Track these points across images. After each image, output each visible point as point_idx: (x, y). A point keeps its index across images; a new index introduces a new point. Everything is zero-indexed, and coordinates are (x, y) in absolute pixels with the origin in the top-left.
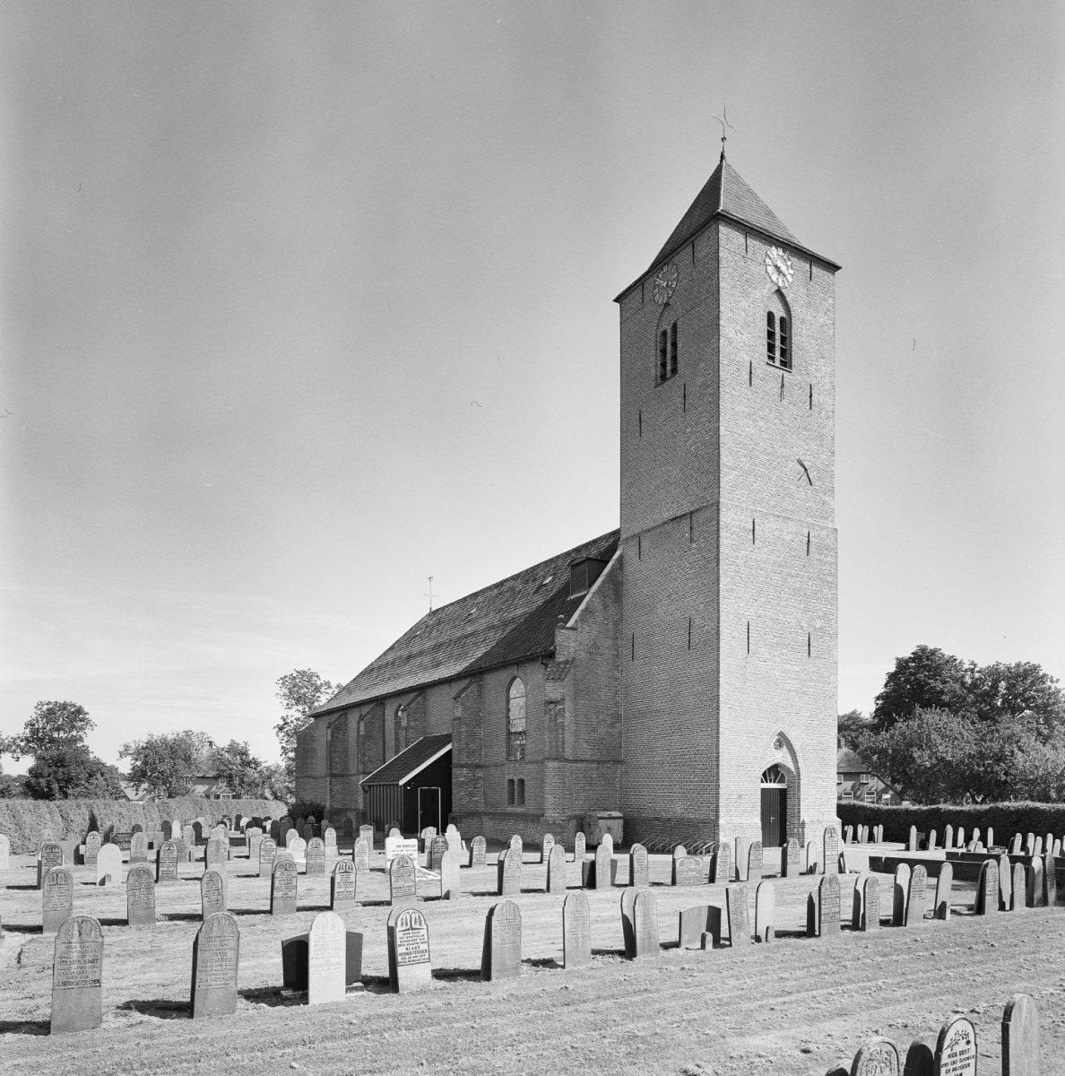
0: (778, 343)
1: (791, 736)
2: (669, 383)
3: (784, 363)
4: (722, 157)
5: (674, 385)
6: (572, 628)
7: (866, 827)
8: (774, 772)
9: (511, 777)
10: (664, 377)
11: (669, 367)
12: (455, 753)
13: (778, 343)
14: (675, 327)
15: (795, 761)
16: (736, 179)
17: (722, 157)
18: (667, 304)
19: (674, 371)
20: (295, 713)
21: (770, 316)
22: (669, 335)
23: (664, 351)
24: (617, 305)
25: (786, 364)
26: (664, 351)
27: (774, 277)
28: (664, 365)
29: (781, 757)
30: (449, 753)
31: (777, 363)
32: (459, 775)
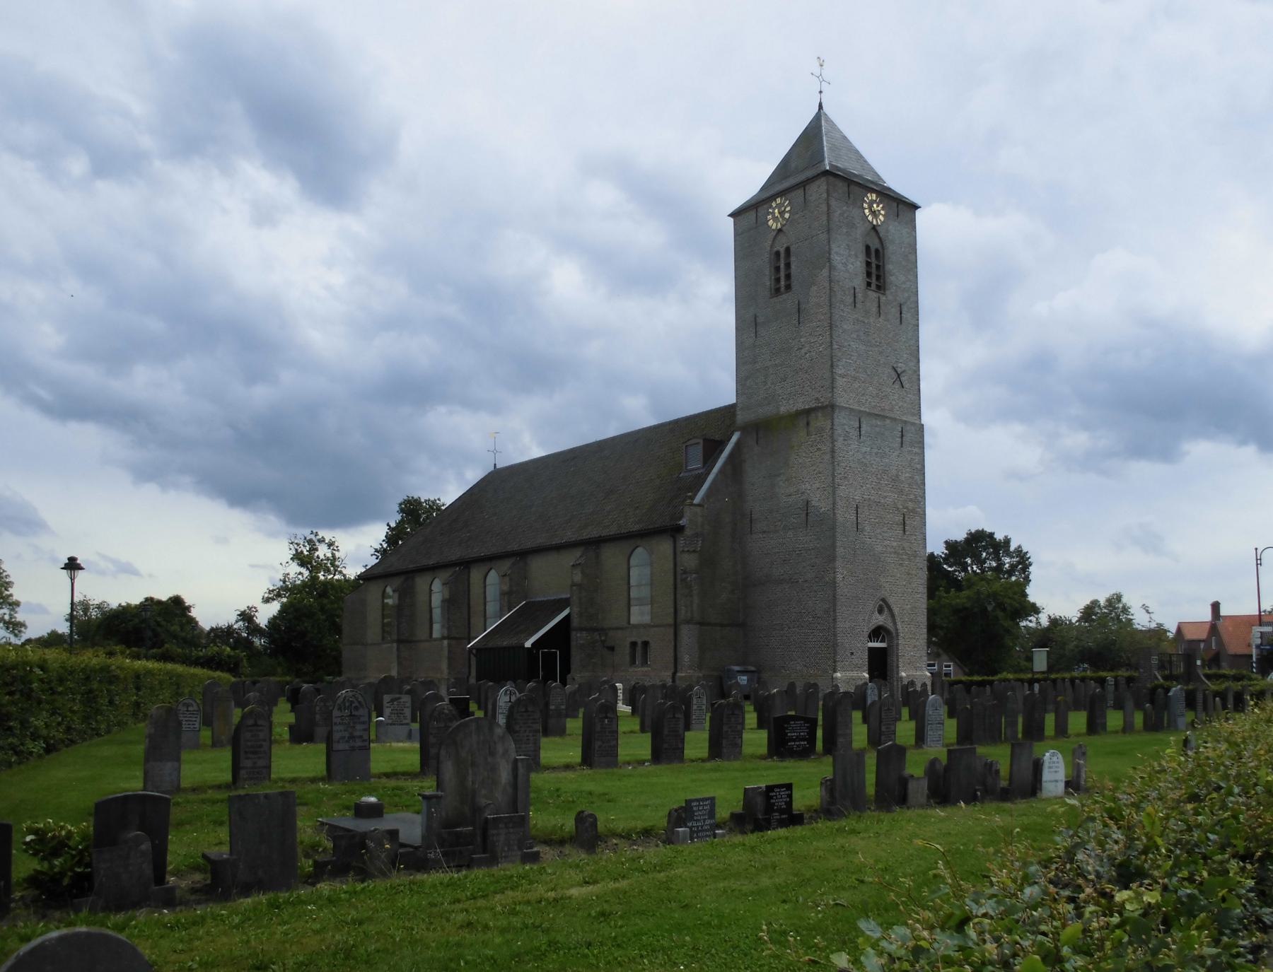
0: (874, 270)
1: (891, 601)
2: (781, 298)
3: (879, 287)
4: (821, 106)
5: (788, 300)
6: (699, 505)
7: (87, 825)
8: (877, 633)
9: (633, 639)
10: (778, 291)
11: (783, 283)
12: (575, 622)
13: (874, 270)
14: (788, 250)
15: (895, 624)
16: (828, 120)
17: (821, 106)
18: (780, 230)
19: (788, 287)
20: (296, 572)
21: (868, 248)
22: (782, 255)
23: (777, 269)
24: (732, 220)
25: (881, 288)
26: (777, 269)
27: (870, 218)
28: (778, 280)
29: (880, 620)
30: (567, 618)
31: (873, 286)
32: (578, 638)
